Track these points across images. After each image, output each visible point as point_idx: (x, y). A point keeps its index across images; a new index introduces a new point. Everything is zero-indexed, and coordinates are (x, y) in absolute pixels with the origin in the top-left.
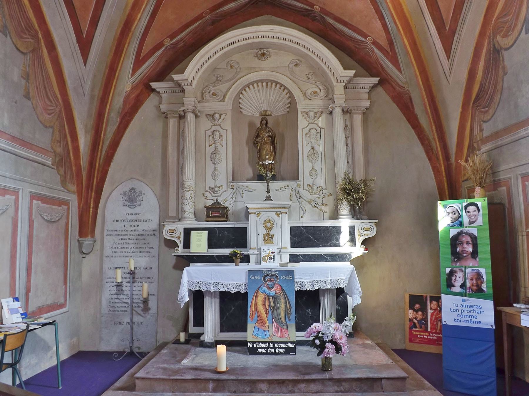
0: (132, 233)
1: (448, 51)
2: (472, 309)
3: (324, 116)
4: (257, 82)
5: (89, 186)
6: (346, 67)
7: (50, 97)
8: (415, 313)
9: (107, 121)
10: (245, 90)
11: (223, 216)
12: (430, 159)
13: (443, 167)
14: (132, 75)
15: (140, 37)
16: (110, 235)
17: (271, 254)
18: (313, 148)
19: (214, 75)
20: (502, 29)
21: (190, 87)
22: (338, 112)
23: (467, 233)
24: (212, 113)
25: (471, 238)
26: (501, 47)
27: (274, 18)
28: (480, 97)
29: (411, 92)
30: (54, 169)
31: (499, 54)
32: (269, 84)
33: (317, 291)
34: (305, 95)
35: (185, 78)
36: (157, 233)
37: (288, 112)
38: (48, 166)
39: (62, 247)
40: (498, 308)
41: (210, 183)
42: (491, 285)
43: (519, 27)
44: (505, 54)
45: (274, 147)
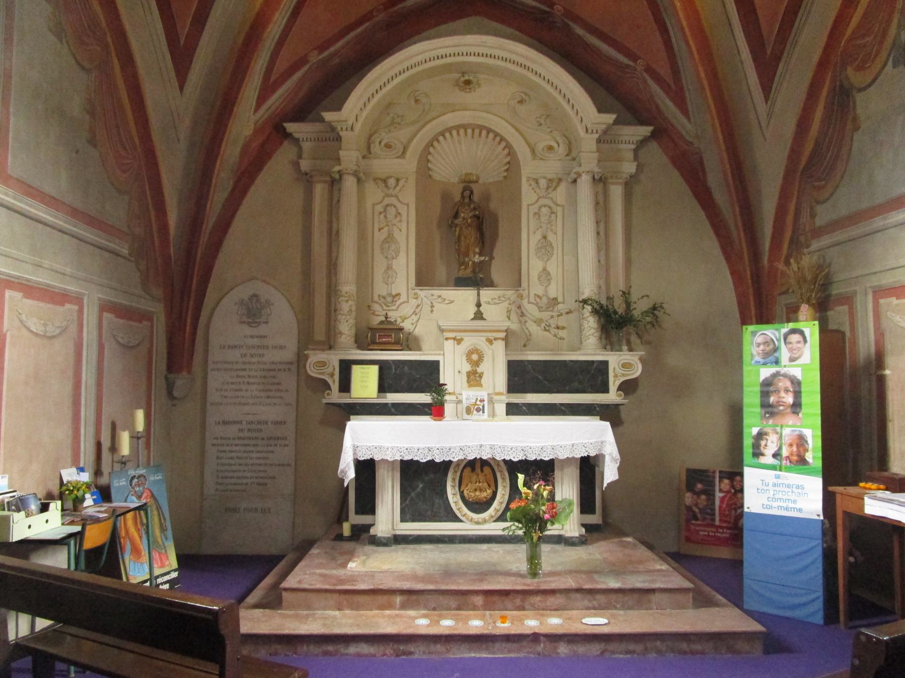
0: (254, 367)
1: (767, 87)
3: (562, 188)
4: (458, 128)
6: (602, 109)
8: (695, 496)
10: (438, 141)
11: (397, 342)
12: (728, 259)
13: (749, 273)
14: (256, 111)
16: (218, 370)
17: (478, 403)
18: (545, 237)
19: (387, 114)
21: (349, 133)
23: (785, 376)
24: (384, 176)
25: (792, 382)
27: (495, 25)
31: (848, 96)
32: (477, 131)
33: (552, 461)
34: (533, 151)
36: (294, 368)
37: (505, 177)
40: (831, 489)
42: (820, 454)
43: (884, 54)
44: (859, 98)
45: (482, 234)
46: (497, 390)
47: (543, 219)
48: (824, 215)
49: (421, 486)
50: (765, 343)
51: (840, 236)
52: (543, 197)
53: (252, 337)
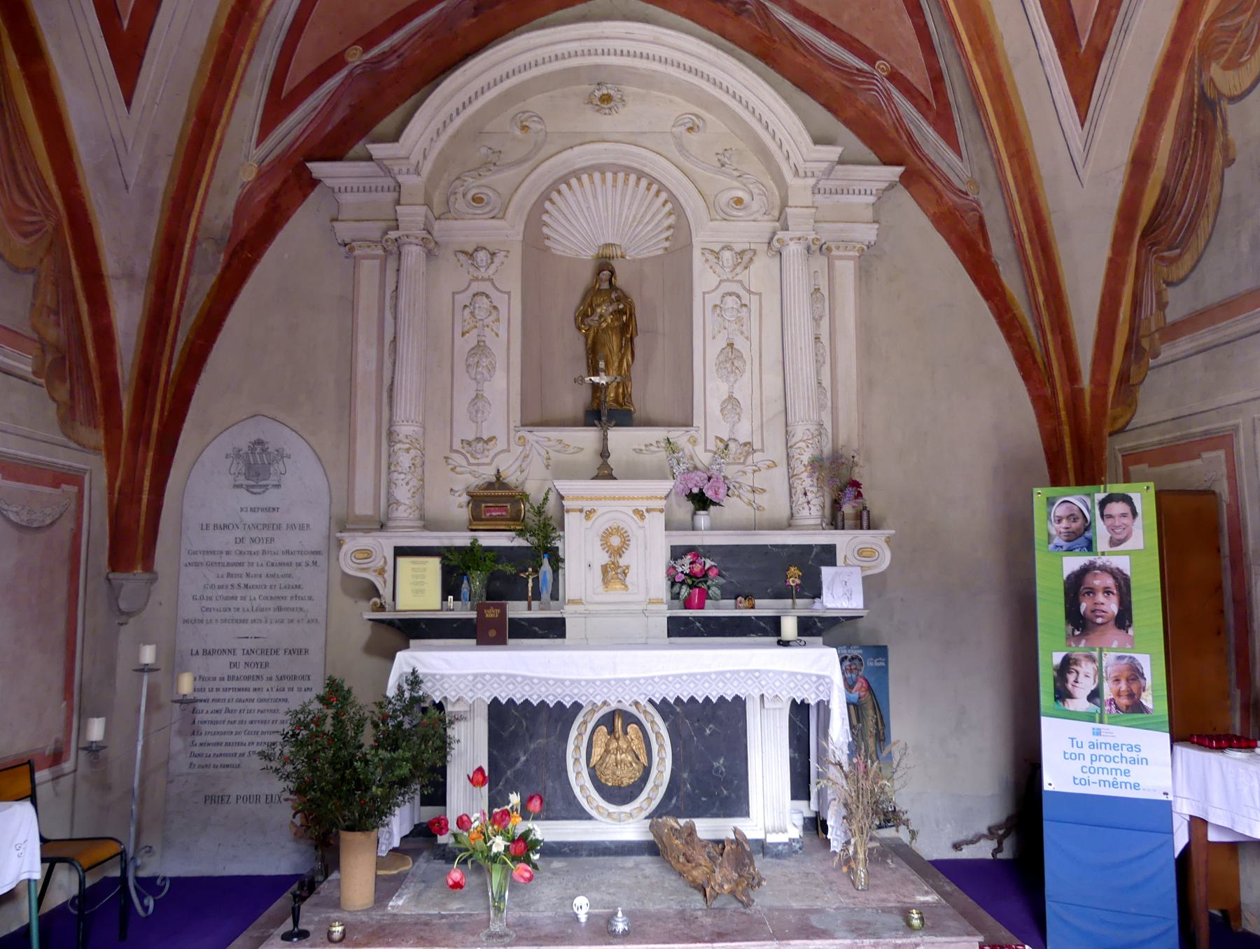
0: (255, 559)
2: (1118, 754)
5: (139, 434)
7: (29, 188)
9: (190, 262)
12: (1026, 378)
14: (260, 141)
15: (282, 38)
16: (197, 564)
18: (731, 345)
20: (1225, 46)
22: (794, 250)
23: (1105, 569)
25: (1115, 578)
26: (1219, 93)
28: (1157, 226)
29: (983, 204)
30: (40, 385)
35: (403, 153)
38: (21, 378)
39: (61, 595)
41: (466, 430)
44: (1230, 110)
46: (653, 595)
47: (728, 315)
48: (1179, 304)
49: (523, 759)
50: (1071, 517)
51: (1206, 337)
52: (728, 280)
53: (253, 510)
